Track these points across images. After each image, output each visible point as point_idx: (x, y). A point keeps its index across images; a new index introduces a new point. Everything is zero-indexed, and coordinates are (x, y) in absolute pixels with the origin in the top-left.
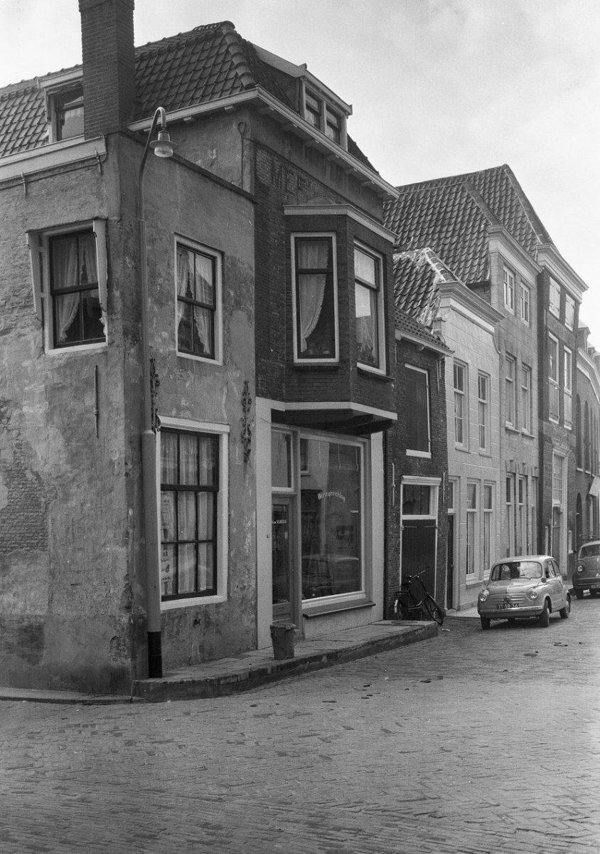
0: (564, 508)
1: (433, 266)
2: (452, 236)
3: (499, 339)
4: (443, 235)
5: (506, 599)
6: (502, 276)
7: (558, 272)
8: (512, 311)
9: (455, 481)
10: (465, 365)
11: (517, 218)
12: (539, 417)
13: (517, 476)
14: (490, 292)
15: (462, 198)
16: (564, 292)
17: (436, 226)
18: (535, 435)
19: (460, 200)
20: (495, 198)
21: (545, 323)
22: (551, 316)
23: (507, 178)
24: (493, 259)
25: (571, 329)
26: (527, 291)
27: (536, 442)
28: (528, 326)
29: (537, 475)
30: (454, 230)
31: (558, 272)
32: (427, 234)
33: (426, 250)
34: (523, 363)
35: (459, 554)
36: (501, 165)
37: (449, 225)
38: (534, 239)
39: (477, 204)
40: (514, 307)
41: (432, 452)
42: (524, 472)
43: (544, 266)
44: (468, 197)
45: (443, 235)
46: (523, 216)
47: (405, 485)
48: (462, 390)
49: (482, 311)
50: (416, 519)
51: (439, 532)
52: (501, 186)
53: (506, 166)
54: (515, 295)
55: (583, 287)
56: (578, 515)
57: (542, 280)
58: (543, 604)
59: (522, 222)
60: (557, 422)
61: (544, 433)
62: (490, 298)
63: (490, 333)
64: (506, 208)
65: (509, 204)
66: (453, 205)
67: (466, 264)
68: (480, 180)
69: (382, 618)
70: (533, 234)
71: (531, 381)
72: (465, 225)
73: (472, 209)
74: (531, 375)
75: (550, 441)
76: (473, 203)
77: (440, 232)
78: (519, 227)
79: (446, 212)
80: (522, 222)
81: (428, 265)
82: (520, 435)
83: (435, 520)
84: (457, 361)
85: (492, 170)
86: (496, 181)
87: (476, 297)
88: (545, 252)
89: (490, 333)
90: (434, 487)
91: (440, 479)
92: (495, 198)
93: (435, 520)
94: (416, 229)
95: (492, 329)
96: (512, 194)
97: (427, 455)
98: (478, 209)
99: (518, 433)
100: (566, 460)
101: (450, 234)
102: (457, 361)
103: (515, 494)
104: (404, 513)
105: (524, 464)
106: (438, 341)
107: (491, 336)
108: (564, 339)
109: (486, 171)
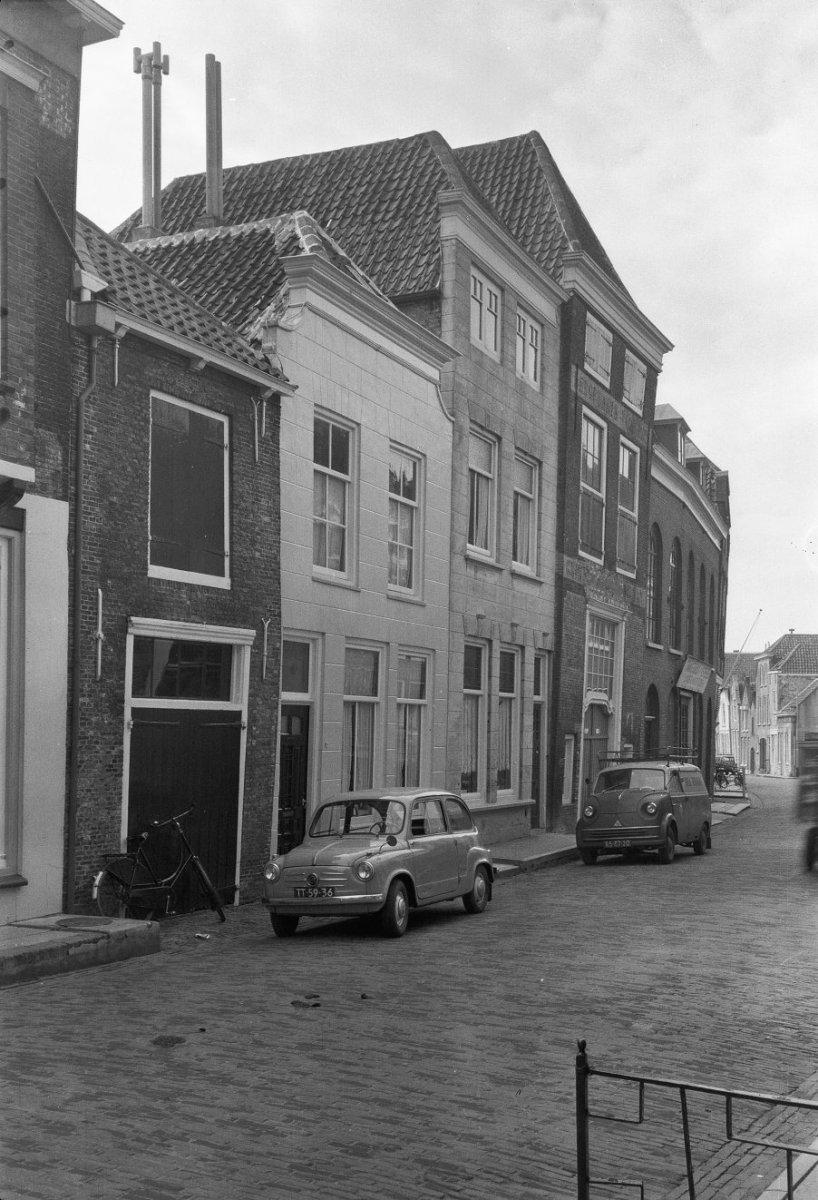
0: (616, 706)
1: (303, 239)
2: (394, 218)
3: (452, 401)
4: (380, 217)
5: (311, 878)
6: (462, 283)
7: (595, 295)
8: (535, 386)
9: (314, 640)
10: (354, 426)
11: (541, 215)
12: (557, 548)
13: (496, 645)
14: (440, 312)
15: (420, 157)
16: (620, 345)
17: (370, 202)
18: (548, 577)
19: (417, 161)
20: (511, 183)
21: (573, 388)
22: (587, 378)
23: (534, 153)
24: (448, 251)
25: (640, 412)
26: (537, 327)
27: (548, 591)
28: (538, 390)
29: (549, 646)
30: (398, 208)
31: (595, 295)
32: (355, 215)
33: (297, 215)
34: (517, 448)
35: (319, 780)
36: (526, 131)
37: (392, 200)
38: (564, 248)
39: (443, 167)
40: (538, 378)
41: (231, 576)
42: (514, 638)
43: (573, 290)
44: (432, 155)
45: (380, 217)
46: (552, 213)
47: (138, 640)
48: (345, 470)
49: (410, 338)
50: (219, 708)
51: (250, 734)
52: (522, 164)
53: (535, 135)
54: (503, 328)
55: (665, 346)
56: (649, 723)
57: (572, 316)
58: (386, 892)
59: (549, 222)
60: (601, 562)
61: (565, 575)
62: (440, 322)
63: (429, 379)
64: (526, 199)
65: (531, 192)
66: (405, 169)
67: (406, 263)
68: (492, 155)
69: (60, 910)
70: (564, 240)
71: (540, 483)
72: (418, 200)
73: (434, 174)
74: (540, 475)
75: (581, 589)
76: (437, 164)
77: (376, 212)
78: (543, 228)
79: (391, 180)
80: (549, 222)
81: (295, 238)
82: (505, 573)
83: (240, 713)
84: (320, 411)
85: (512, 141)
86: (517, 156)
87: (408, 321)
88: (577, 266)
89: (429, 379)
90: (240, 647)
91: (253, 632)
92: (511, 183)
93: (240, 713)
94: (338, 208)
95: (434, 374)
96: (539, 178)
97: (223, 583)
98: (444, 174)
99: (501, 570)
100: (622, 628)
101: (390, 215)
102: (320, 411)
103: (490, 677)
104: (135, 694)
105: (513, 625)
106: (266, 366)
107: (431, 387)
108: (619, 423)
109: (503, 142)
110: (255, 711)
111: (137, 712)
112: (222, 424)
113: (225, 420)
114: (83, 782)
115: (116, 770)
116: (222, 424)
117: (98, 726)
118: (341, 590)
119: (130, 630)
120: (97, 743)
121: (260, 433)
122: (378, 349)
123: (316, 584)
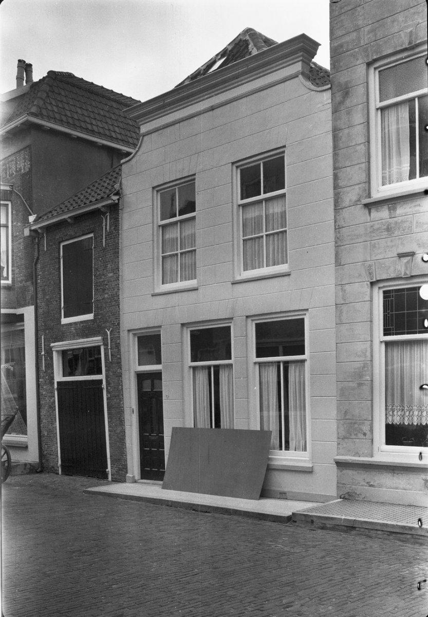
110: (109, 379)
111: (100, 372)
112: (63, 246)
113: (62, 245)
114: (43, 412)
115: (52, 408)
116: (63, 246)
117: (46, 390)
118: (186, 293)
119: (53, 349)
120: (46, 397)
121: (106, 229)
122: (212, 109)
123: (154, 298)
